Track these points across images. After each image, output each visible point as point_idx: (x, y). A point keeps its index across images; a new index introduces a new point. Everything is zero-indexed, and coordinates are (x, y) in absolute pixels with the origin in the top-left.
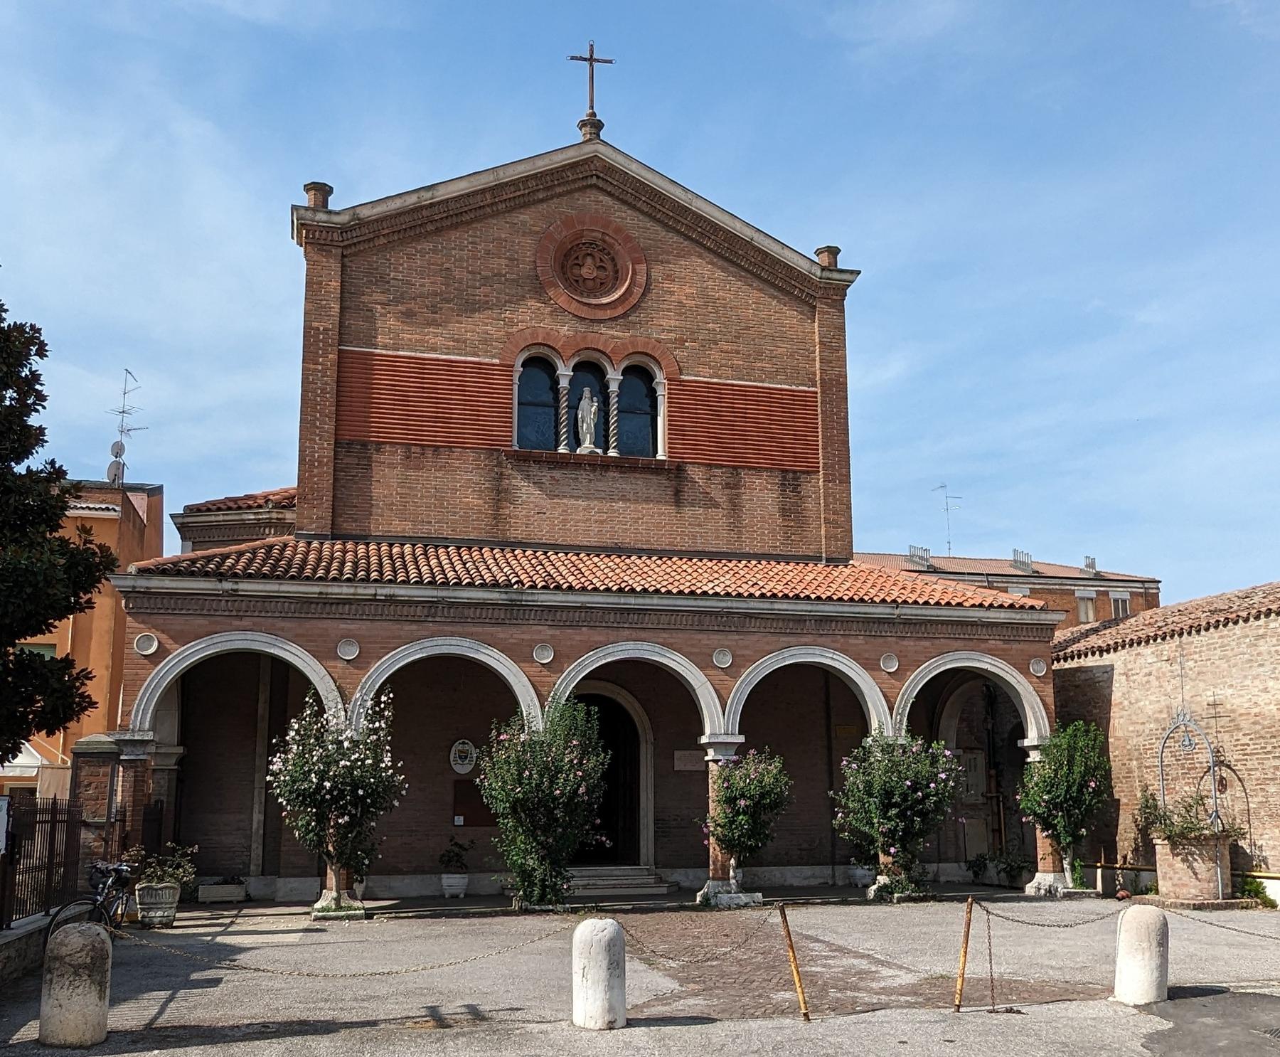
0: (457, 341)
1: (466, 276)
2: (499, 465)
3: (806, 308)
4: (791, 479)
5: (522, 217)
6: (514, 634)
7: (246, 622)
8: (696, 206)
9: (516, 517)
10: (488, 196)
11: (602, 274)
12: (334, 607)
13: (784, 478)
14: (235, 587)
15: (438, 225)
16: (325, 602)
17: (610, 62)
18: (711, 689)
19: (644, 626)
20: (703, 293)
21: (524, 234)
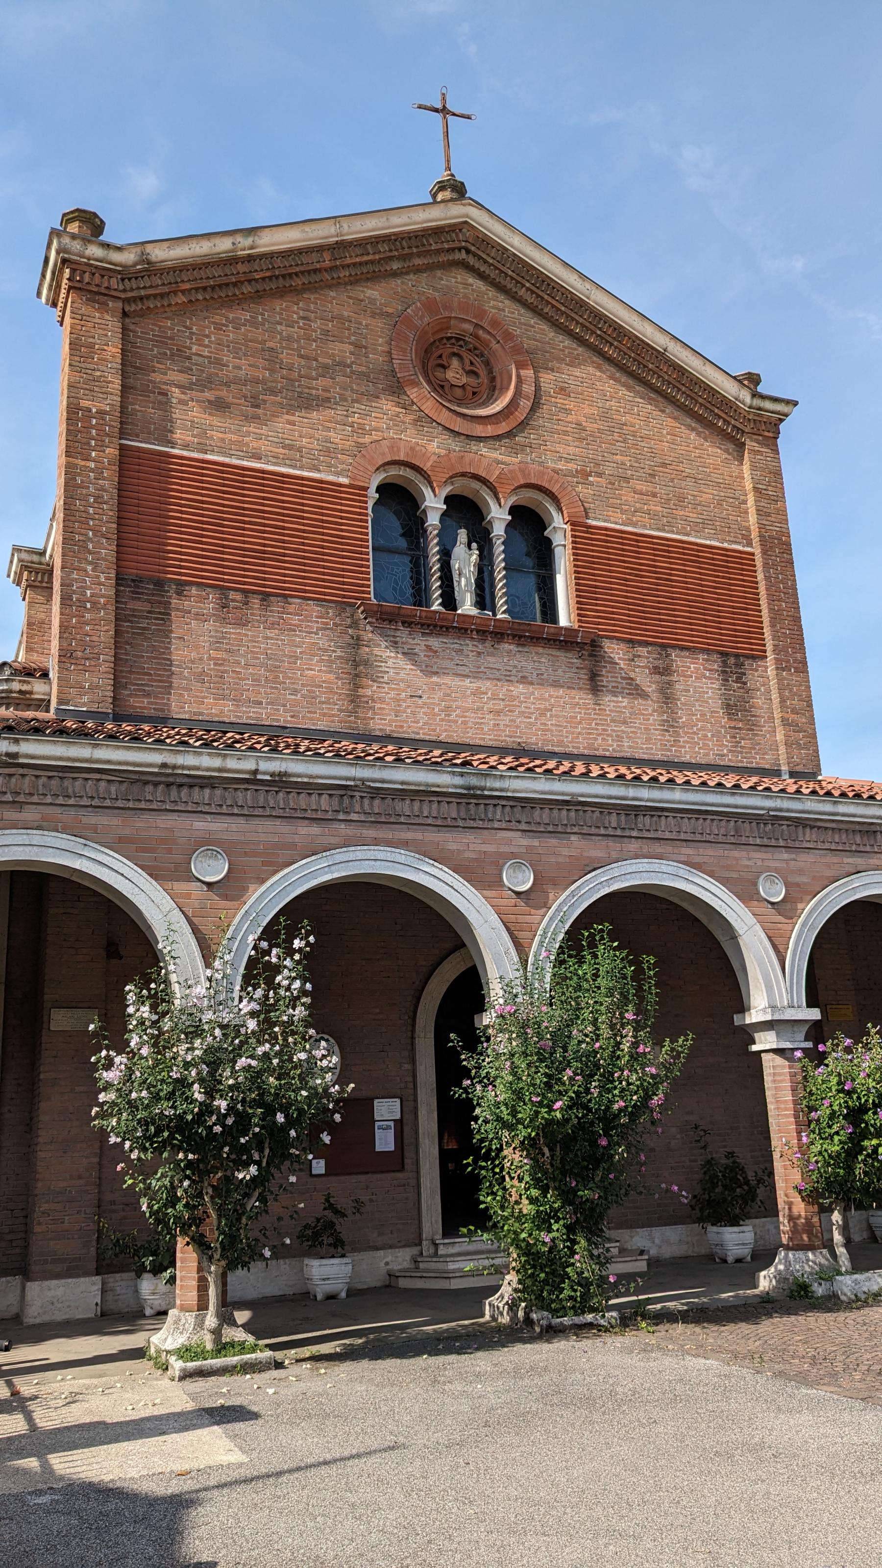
0: (290, 447)
1: (297, 361)
2: (355, 624)
3: (731, 447)
4: (735, 660)
5: (369, 293)
6: (470, 844)
7: (30, 814)
8: (596, 299)
9: (382, 700)
10: (327, 256)
11: (472, 381)
12: (185, 791)
13: (725, 664)
14: (13, 749)
15: (259, 287)
16: (170, 781)
17: (469, 118)
18: (763, 935)
19: (659, 834)
20: (605, 415)
21: (373, 315)
